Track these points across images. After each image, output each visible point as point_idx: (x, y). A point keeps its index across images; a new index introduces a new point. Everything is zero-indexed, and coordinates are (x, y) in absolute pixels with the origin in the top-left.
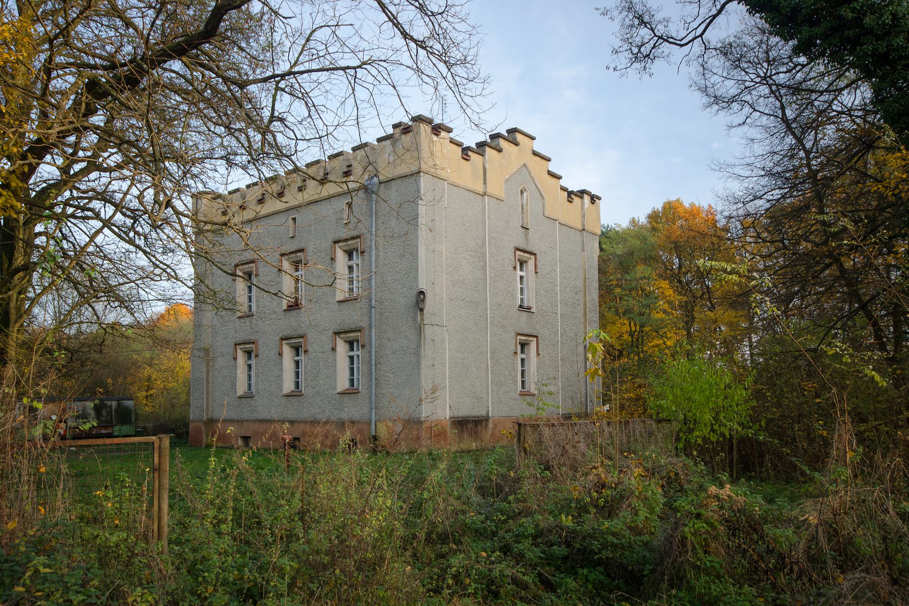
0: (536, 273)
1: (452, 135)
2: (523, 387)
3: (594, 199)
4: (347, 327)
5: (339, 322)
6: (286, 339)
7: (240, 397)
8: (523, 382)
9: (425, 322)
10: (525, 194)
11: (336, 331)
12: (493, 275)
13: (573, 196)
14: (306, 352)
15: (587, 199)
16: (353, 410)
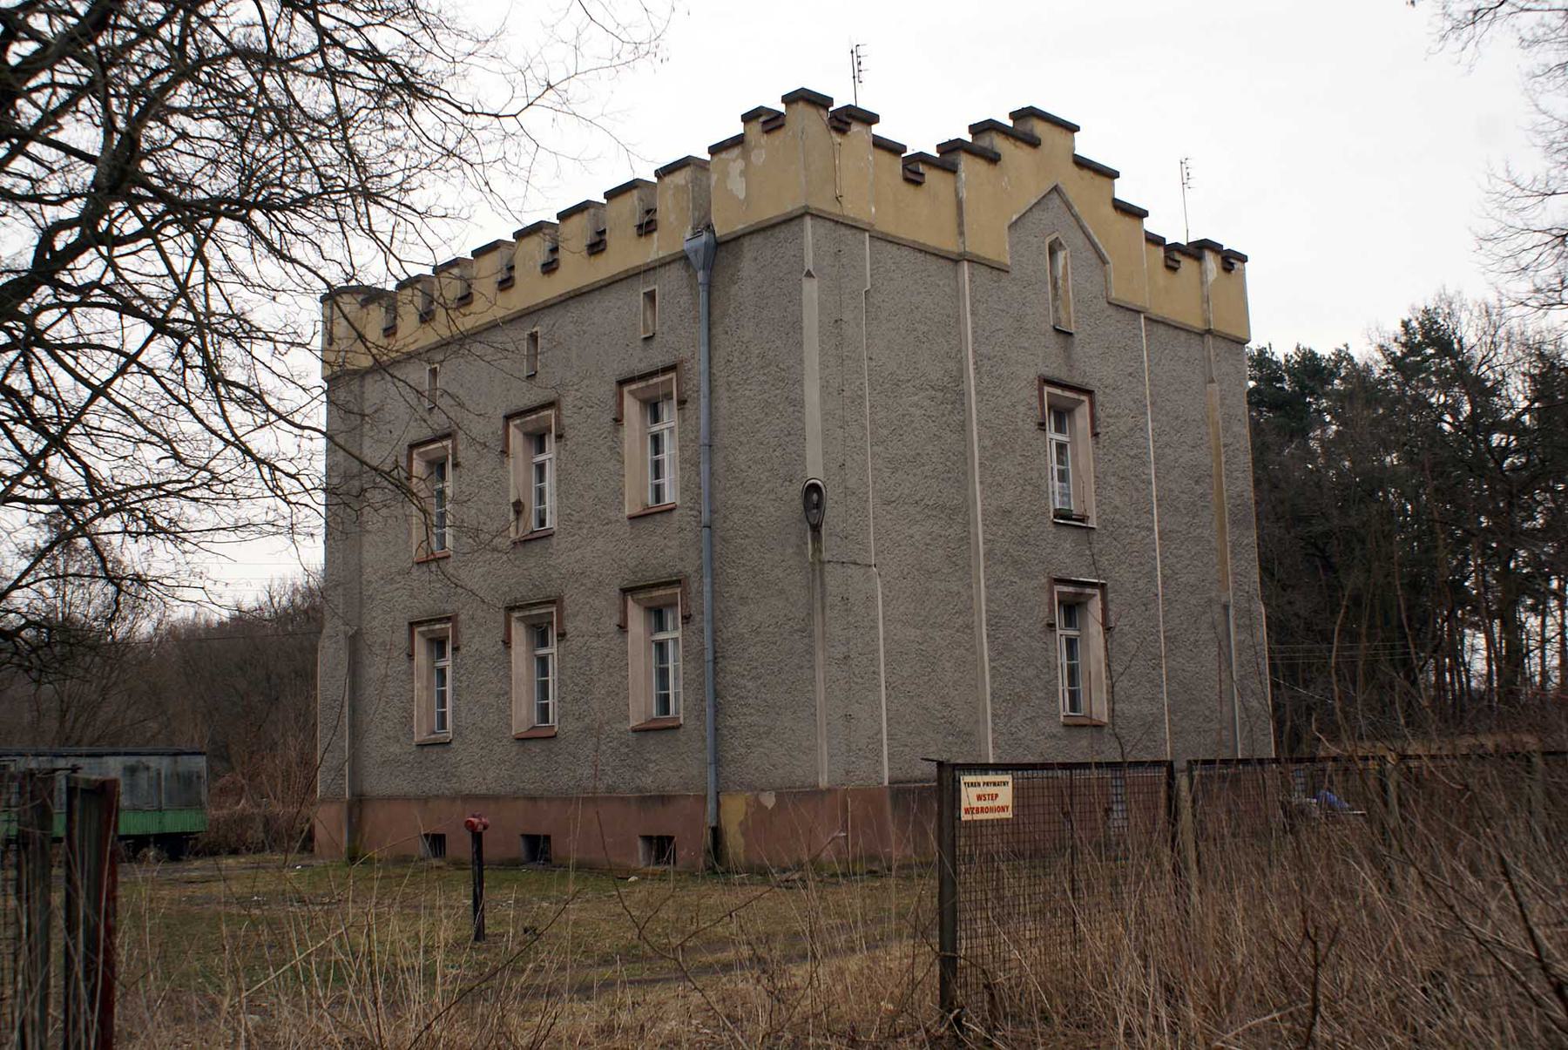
0: (1095, 435)
1: (876, 129)
2: (1074, 706)
3: (1231, 261)
4: (650, 577)
5: (632, 563)
6: (520, 608)
7: (421, 746)
8: (1074, 696)
9: (826, 556)
10: (1061, 255)
11: (625, 584)
12: (988, 443)
13: (1178, 256)
14: (562, 636)
15: (1212, 262)
16: (669, 769)
